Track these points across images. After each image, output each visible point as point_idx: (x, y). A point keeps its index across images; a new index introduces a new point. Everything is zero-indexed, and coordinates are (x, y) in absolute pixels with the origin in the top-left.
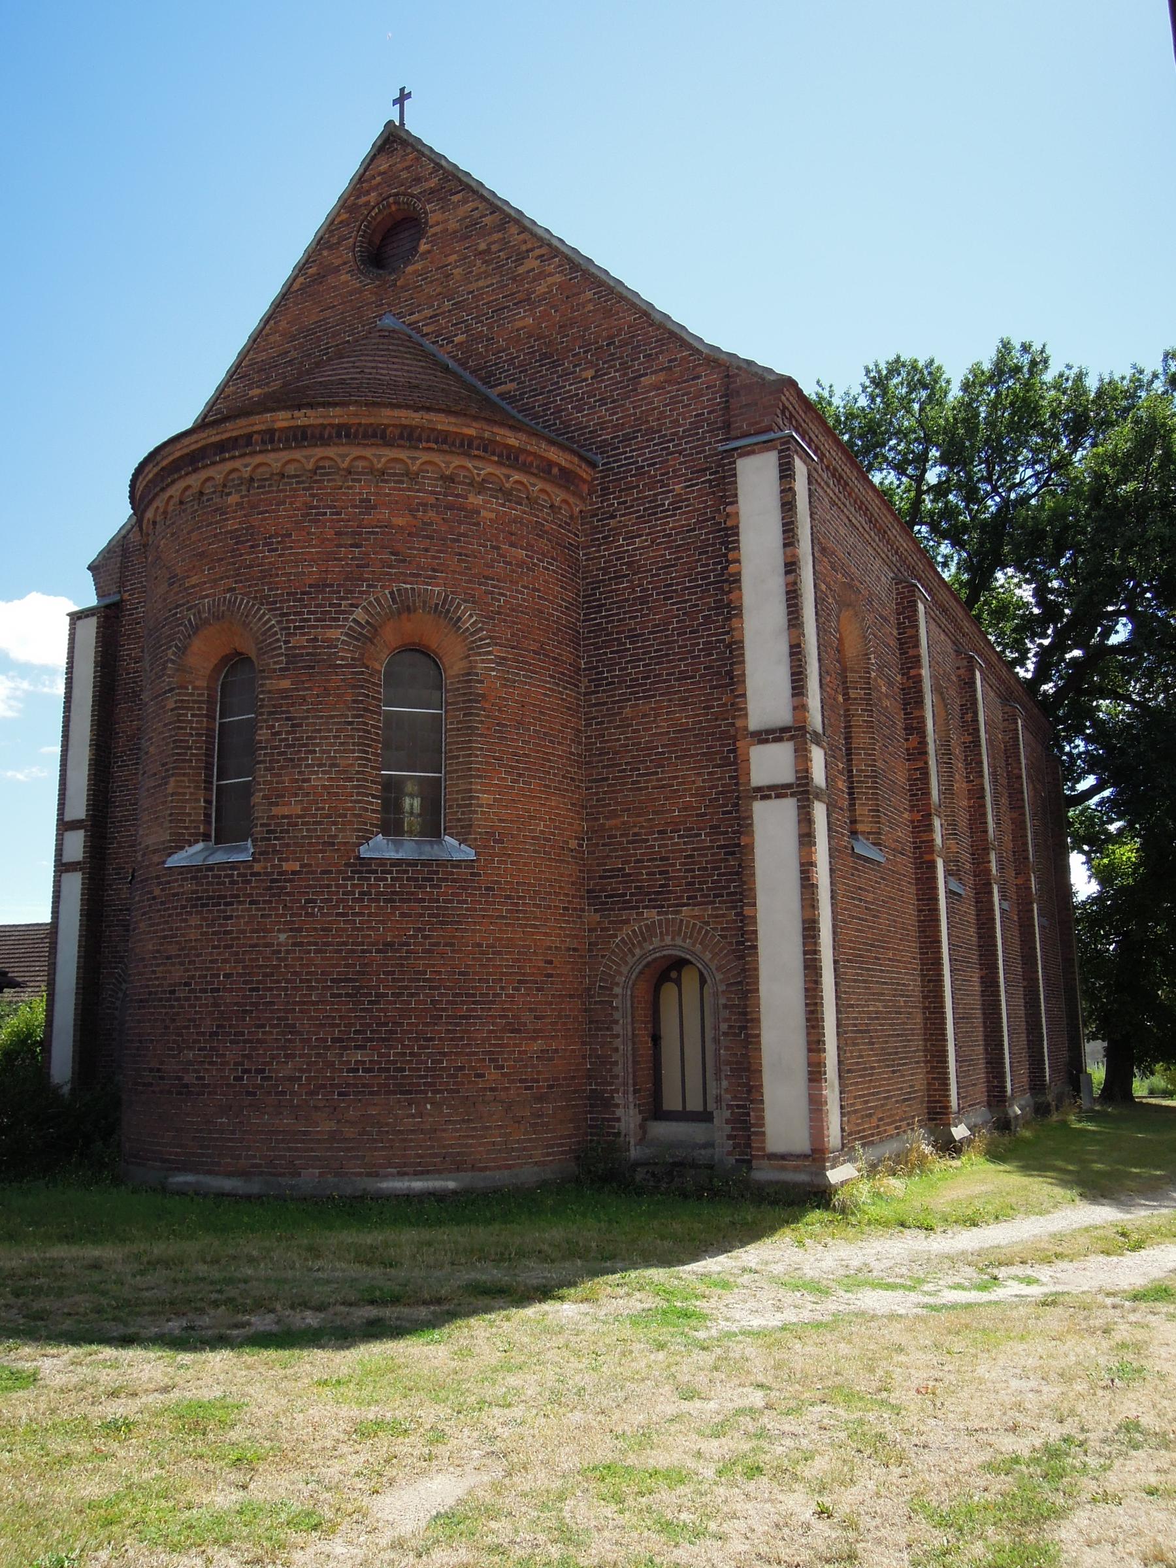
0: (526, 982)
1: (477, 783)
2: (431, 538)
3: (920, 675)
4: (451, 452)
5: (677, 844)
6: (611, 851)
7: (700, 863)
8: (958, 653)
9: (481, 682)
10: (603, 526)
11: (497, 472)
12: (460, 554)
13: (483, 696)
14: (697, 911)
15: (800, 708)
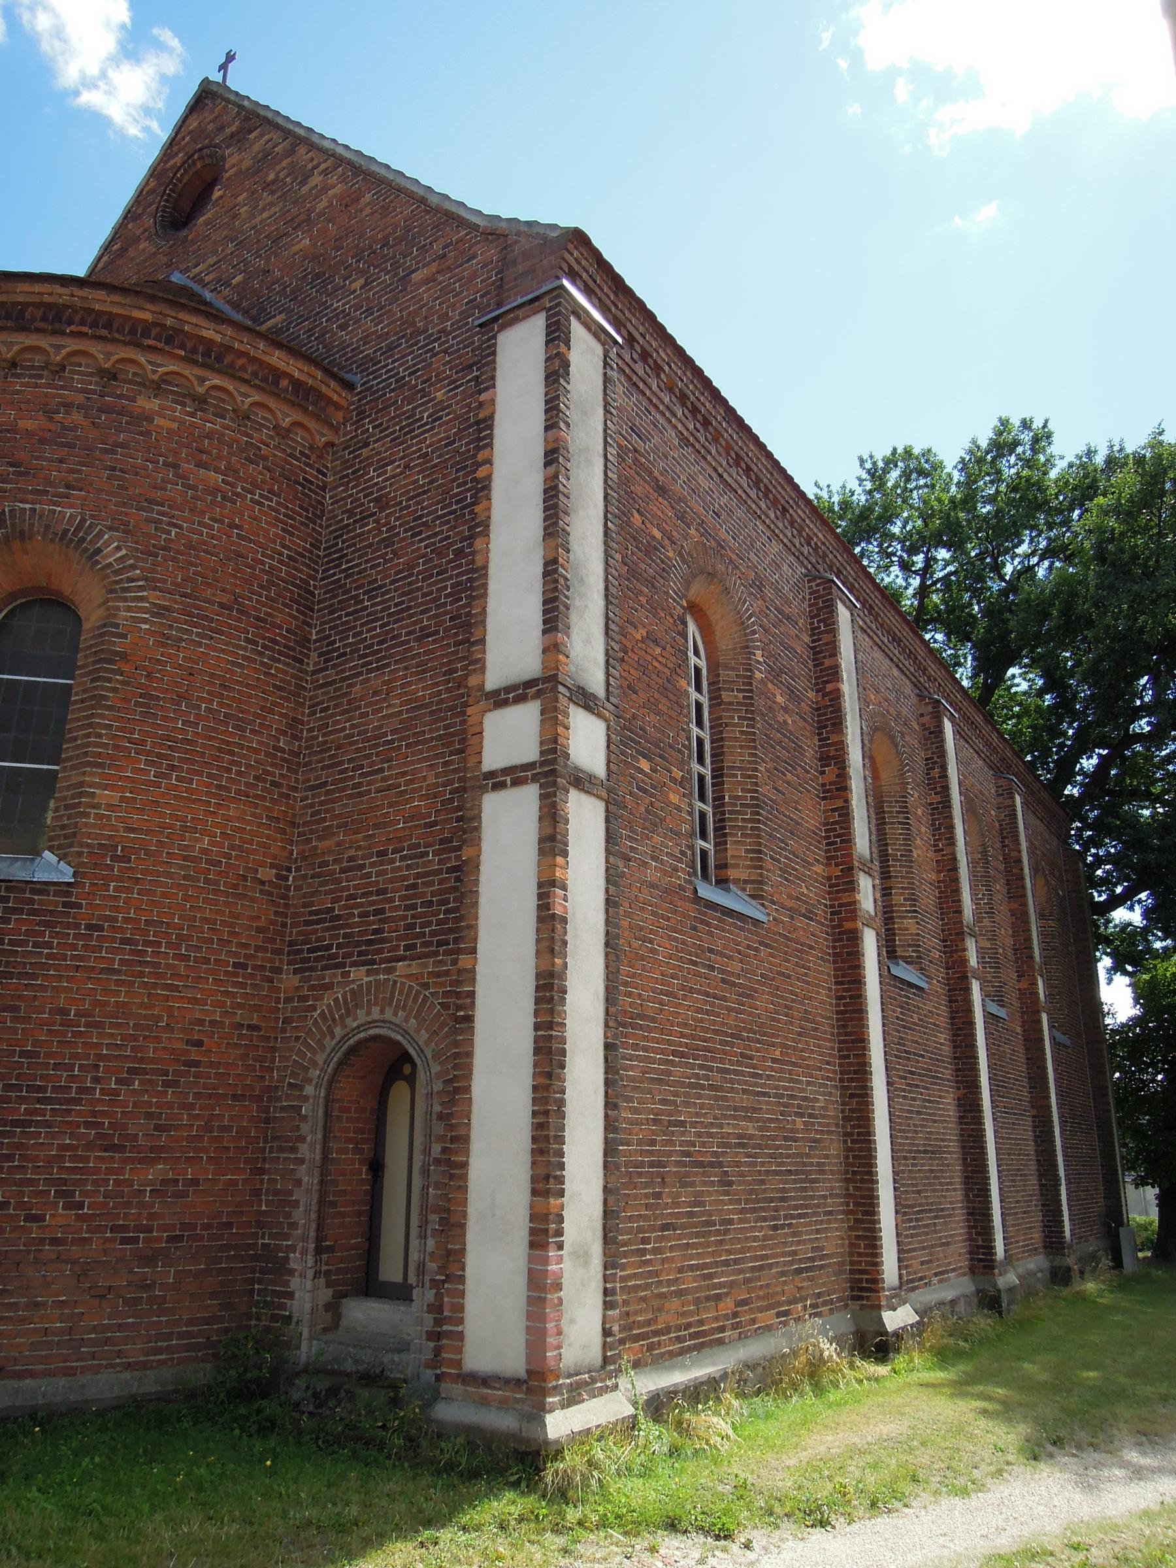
0: (144, 1071)
1: (92, 774)
2: (72, 446)
3: (838, 690)
4: (114, 341)
5: (399, 869)
6: (322, 884)
7: (424, 895)
8: (921, 697)
9: (124, 636)
10: (355, 458)
11: (186, 372)
12: (113, 469)
13: (124, 656)
14: (415, 967)
15: (553, 649)
